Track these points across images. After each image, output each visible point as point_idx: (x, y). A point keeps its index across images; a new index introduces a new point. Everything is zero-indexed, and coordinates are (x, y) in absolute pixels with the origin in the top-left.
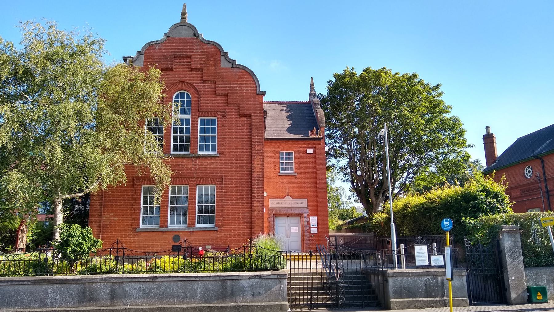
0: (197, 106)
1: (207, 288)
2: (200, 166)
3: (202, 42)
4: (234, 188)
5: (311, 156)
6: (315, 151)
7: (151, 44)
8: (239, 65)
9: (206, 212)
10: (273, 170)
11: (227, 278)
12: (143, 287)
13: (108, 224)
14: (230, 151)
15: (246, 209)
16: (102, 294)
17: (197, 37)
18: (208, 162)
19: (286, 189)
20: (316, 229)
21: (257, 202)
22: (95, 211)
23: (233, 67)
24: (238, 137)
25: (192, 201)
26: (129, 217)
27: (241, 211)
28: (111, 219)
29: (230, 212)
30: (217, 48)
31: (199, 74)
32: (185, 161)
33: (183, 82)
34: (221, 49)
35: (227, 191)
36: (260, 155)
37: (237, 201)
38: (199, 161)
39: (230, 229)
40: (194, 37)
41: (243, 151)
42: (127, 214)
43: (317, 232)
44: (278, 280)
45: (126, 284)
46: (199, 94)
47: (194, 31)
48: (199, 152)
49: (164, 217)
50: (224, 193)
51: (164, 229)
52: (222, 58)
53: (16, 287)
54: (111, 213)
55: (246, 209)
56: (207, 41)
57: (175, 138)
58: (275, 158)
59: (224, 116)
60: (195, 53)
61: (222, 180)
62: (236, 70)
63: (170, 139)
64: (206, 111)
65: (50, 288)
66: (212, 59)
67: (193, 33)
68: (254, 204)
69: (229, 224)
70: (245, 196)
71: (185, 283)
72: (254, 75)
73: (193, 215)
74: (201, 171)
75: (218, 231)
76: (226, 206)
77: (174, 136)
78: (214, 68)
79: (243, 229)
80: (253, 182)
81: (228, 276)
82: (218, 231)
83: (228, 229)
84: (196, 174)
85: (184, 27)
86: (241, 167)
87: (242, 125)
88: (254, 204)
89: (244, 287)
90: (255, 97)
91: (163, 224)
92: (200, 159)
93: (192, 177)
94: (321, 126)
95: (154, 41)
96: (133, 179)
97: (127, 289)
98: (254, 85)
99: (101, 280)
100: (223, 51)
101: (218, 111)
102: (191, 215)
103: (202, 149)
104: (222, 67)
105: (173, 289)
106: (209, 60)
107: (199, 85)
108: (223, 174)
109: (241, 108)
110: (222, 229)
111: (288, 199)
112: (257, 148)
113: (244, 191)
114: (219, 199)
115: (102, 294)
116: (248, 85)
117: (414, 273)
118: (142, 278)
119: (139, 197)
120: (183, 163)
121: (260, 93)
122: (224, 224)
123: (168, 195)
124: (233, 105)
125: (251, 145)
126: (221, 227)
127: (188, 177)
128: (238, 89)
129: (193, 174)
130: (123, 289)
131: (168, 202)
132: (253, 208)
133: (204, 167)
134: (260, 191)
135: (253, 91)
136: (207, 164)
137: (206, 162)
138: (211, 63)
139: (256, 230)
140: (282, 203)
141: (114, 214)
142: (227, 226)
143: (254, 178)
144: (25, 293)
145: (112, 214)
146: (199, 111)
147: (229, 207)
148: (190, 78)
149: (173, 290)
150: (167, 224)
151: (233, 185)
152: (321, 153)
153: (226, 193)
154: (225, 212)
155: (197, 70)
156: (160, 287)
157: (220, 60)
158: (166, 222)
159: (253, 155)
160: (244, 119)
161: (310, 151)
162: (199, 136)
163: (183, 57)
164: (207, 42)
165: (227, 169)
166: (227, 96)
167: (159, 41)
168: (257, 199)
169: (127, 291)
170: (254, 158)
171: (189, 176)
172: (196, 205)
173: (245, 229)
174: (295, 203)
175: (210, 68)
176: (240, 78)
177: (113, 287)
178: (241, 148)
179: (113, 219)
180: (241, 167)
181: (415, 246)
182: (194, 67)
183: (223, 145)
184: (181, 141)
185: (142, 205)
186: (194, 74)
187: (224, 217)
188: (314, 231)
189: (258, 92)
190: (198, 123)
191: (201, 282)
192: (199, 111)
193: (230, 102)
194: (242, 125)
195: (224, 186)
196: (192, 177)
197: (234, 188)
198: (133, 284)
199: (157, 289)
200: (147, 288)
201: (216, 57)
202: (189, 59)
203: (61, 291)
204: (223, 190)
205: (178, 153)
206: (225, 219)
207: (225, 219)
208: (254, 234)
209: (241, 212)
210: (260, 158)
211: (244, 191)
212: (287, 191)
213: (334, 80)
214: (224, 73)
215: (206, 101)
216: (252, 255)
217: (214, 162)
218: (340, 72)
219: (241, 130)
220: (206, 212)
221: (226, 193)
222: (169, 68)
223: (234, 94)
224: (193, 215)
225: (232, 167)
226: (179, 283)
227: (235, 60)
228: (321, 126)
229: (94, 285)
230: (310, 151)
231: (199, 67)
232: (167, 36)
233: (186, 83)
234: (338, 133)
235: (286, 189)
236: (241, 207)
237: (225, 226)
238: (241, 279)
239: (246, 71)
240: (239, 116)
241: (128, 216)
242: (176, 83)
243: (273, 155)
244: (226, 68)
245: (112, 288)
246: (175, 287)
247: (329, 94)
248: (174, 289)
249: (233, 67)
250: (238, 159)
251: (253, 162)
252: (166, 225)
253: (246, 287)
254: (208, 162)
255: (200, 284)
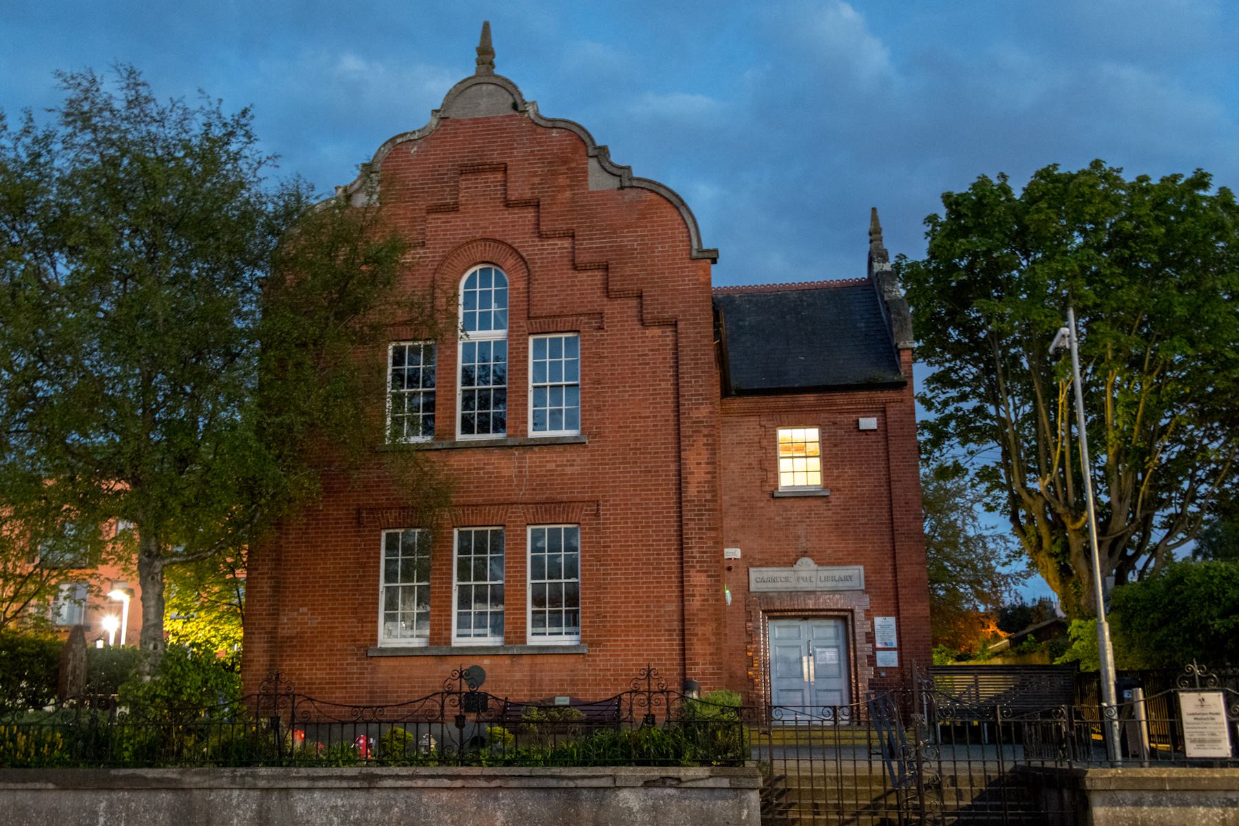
0: (524, 306)
1: (523, 811)
2: (535, 471)
3: (536, 124)
4: (632, 532)
5: (873, 438)
6: (884, 423)
7: (399, 140)
8: (639, 179)
9: (555, 601)
10: (758, 483)
11: (580, 783)
12: (343, 806)
13: (295, 637)
14: (620, 427)
15: (668, 592)
16: (235, 821)
17: (522, 112)
18: (555, 461)
19: (797, 538)
20: (894, 655)
21: (697, 571)
22: (259, 601)
23: (622, 188)
24: (639, 386)
25: (515, 572)
26: (349, 618)
27: (655, 597)
28: (301, 624)
29: (622, 603)
30: (579, 138)
31: (529, 214)
32: (495, 457)
33: (486, 240)
34: (587, 140)
35: (611, 542)
36: (705, 436)
37: (642, 569)
38: (532, 459)
39: (622, 650)
40: (512, 112)
41: (654, 426)
42: (343, 609)
43: (895, 664)
44: (731, 791)
45: (298, 796)
46: (529, 271)
47: (512, 95)
48: (532, 434)
49: (441, 616)
50: (604, 547)
51: (444, 650)
52: (593, 164)
53: (20, 796)
54: (302, 606)
55: (668, 592)
56: (549, 120)
57: (468, 400)
58: (761, 448)
59: (601, 328)
60: (515, 157)
61: (598, 510)
62: (630, 195)
63: (454, 399)
64: (550, 317)
65: (101, 802)
66: (563, 169)
67: (511, 101)
68: (689, 576)
69: (620, 636)
70: (664, 554)
71: (460, 793)
72: (683, 203)
73: (518, 609)
74: (537, 485)
75: (589, 656)
76: (609, 584)
77: (464, 391)
78: (568, 194)
79: (660, 650)
80: (687, 515)
81: (583, 777)
82: (589, 656)
83: (617, 650)
84: (524, 494)
85: (484, 87)
86: (650, 471)
87: (652, 350)
88: (689, 576)
89: (630, 809)
90: (687, 267)
91: (439, 636)
92: (535, 453)
93: (512, 504)
94: (899, 347)
95: (405, 134)
96: (359, 512)
97: (300, 809)
98: (682, 233)
99: (232, 783)
100: (593, 143)
101: (581, 315)
102: (514, 609)
103: (538, 425)
104: (591, 189)
105: (426, 811)
106: (554, 174)
107: (529, 246)
108: (600, 492)
109: (647, 301)
110: (600, 651)
111: (806, 566)
112: (695, 414)
113: (660, 540)
114: (590, 565)
115: (235, 821)
116: (666, 234)
117: (1179, 779)
118: (342, 778)
119: (374, 562)
120: (488, 464)
121: (700, 255)
122: (605, 636)
123: (452, 556)
124: (623, 295)
125: (678, 405)
126: (598, 644)
127: (503, 504)
128: (636, 249)
129: (516, 495)
130: (291, 808)
131: (525, 600)
132: (689, 590)
133: (546, 476)
134: (707, 538)
135: (681, 250)
136: (552, 466)
137: (551, 461)
138: (562, 180)
139: (695, 654)
140: (787, 579)
141: (309, 610)
142: (615, 641)
143: (688, 501)
144: (39, 813)
145: (304, 610)
146: (529, 318)
147: (620, 588)
148: (503, 227)
149: (427, 816)
150: (450, 634)
151: (627, 523)
152: (901, 428)
153: (609, 547)
154: (609, 603)
155: (523, 204)
156: (391, 807)
157: (585, 172)
158: (446, 629)
159: (685, 437)
160: (657, 331)
161: (869, 423)
162: (530, 388)
163: (483, 171)
164: (550, 124)
165: (610, 478)
166: (607, 269)
167: (419, 131)
168: (697, 562)
169: (301, 814)
170: (688, 445)
171: (505, 500)
172: (525, 581)
173: (665, 650)
174: (827, 579)
175: (560, 196)
176: (643, 216)
177: (262, 804)
178: (649, 417)
179: (307, 623)
180: (650, 471)
181: (1181, 694)
182: (514, 196)
183: (598, 409)
184: (484, 403)
185: (382, 584)
186: (515, 215)
187: (605, 617)
188: (888, 659)
189: (694, 254)
190: (527, 352)
191: (506, 792)
192: (529, 318)
193: (615, 286)
194: (652, 350)
195: (604, 528)
196: (512, 504)
197: (632, 532)
198: (317, 795)
199: (383, 811)
200: (356, 809)
201: (573, 165)
202: (499, 176)
203: (128, 809)
204: (601, 538)
205: (476, 437)
206: (609, 622)
207: (609, 622)
208: (693, 664)
209: (652, 602)
210: (704, 445)
211: (660, 540)
212: (803, 544)
213: (943, 214)
214: (597, 205)
215: (548, 287)
216: (654, 716)
217: (574, 461)
218: (961, 187)
219: (648, 364)
220: (555, 601)
221: (609, 547)
222: (448, 204)
223: (626, 263)
224: (518, 609)
225: (625, 472)
226: (445, 796)
227: (628, 168)
228: (899, 347)
229: (213, 796)
230: (869, 423)
231: (528, 194)
232: (442, 116)
233: (495, 240)
234: (970, 371)
235: (797, 538)
236: (655, 587)
237: (609, 641)
238: (620, 788)
239: (662, 196)
240: (643, 324)
241: (347, 613)
242: (467, 243)
243: (757, 439)
244: (603, 192)
245: (260, 806)
246: (433, 804)
247: (933, 254)
248: (430, 812)
249: (622, 188)
250: (640, 449)
251: (683, 455)
252: (446, 638)
253: (637, 812)
254: (555, 461)
255: (502, 798)
